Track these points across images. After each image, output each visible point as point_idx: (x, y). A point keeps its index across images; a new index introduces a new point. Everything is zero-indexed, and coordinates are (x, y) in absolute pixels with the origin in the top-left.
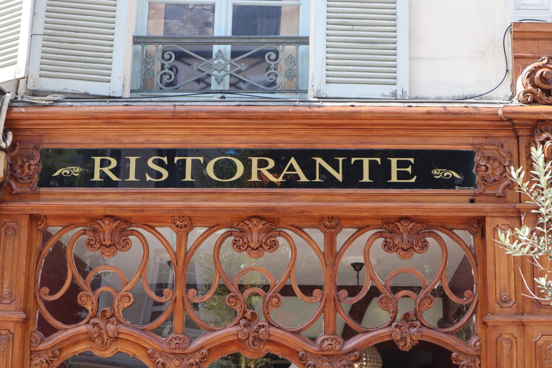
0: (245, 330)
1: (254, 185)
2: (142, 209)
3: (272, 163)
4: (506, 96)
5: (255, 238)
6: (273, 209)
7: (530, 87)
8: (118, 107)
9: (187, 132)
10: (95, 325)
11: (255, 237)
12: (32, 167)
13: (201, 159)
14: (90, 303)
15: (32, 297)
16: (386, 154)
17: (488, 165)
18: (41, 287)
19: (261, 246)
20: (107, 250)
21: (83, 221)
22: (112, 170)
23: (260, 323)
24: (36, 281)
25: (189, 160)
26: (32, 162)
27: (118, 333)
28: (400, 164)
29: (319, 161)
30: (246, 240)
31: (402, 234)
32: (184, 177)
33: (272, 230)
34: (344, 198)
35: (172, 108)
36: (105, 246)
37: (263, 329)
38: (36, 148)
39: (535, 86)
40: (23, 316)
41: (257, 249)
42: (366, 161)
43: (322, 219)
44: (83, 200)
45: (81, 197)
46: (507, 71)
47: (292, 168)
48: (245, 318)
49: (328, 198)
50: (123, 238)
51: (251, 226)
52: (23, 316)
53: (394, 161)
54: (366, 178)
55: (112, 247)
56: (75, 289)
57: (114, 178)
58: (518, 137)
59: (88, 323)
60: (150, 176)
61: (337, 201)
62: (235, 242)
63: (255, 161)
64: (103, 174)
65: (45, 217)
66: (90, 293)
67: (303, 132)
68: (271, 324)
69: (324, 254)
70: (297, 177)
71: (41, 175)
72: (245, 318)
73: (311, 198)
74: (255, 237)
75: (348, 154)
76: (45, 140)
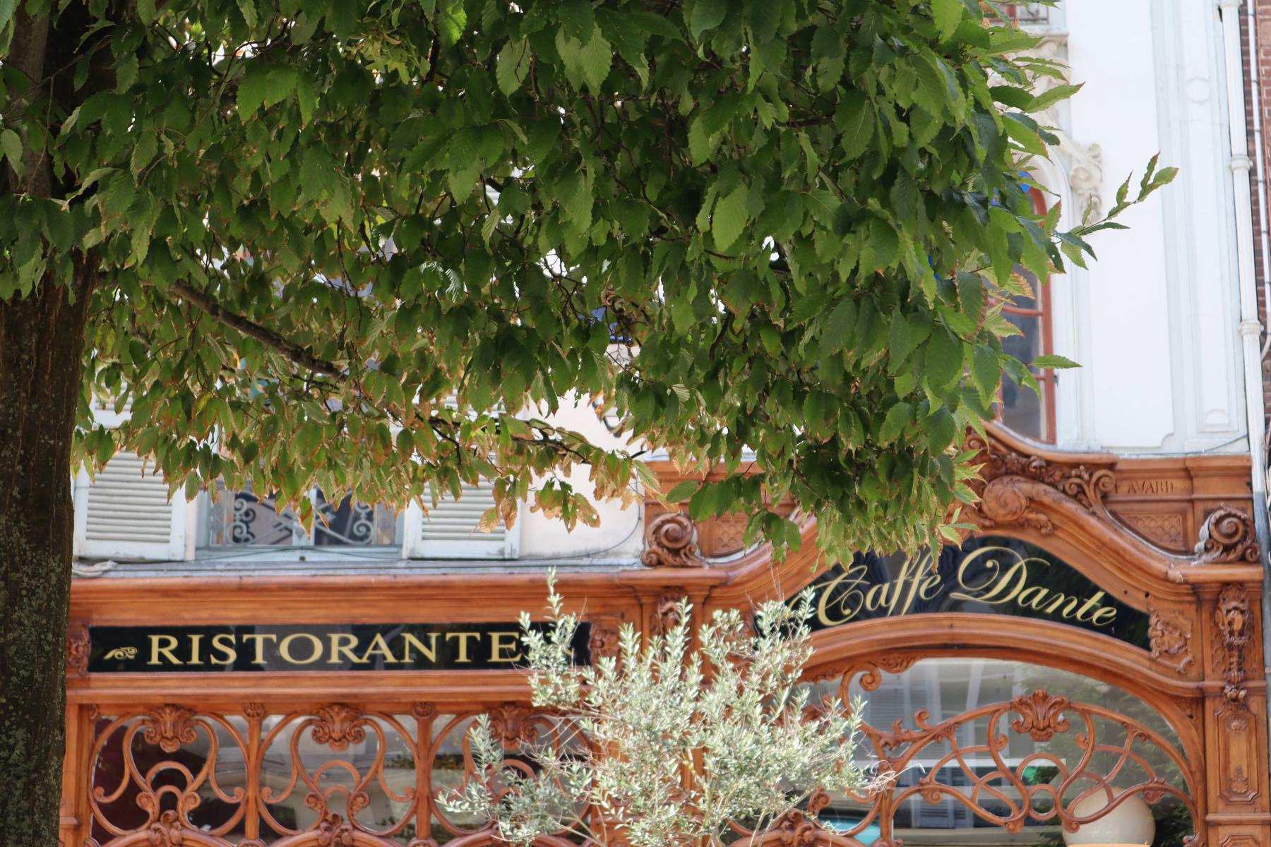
0: (327, 834)
1: (333, 667)
2: (206, 697)
3: (354, 641)
4: (637, 550)
5: (337, 728)
6: (356, 696)
7: (655, 547)
8: (174, 578)
9: (257, 605)
10: (156, 830)
11: (337, 727)
12: (81, 649)
13: (274, 637)
14: (151, 805)
15: (84, 799)
16: (486, 628)
17: (605, 640)
18: (96, 785)
19: (344, 737)
20: (169, 743)
21: (140, 710)
22: (172, 652)
23: (343, 827)
24: (88, 780)
25: (259, 639)
26: (81, 643)
27: (183, 839)
28: (503, 640)
29: (410, 638)
30: (327, 730)
31: (506, 721)
32: (150, 659)
33: (356, 718)
34: (437, 682)
35: (237, 580)
36: (167, 738)
37: (346, 834)
38: (85, 626)
39: (660, 544)
40: (74, 822)
41: (340, 740)
42: (463, 638)
43: (414, 704)
44: (140, 687)
45: (137, 684)
46: (640, 519)
47: (377, 647)
48: (326, 820)
49: (419, 681)
50: (188, 729)
51: (332, 714)
52: (74, 822)
53: (495, 637)
54: (463, 657)
55: (175, 740)
56: (134, 789)
57: (175, 661)
58: (641, 606)
59: (149, 828)
60: (216, 658)
61: (428, 685)
62: (315, 733)
63: (335, 638)
64: (161, 656)
65: (98, 706)
66: (151, 793)
67: (391, 604)
68: (355, 828)
69: (416, 745)
70: (384, 657)
71: (90, 659)
72: (326, 820)
73: (399, 682)
74: (337, 727)
75: (443, 629)
76: (95, 616)
